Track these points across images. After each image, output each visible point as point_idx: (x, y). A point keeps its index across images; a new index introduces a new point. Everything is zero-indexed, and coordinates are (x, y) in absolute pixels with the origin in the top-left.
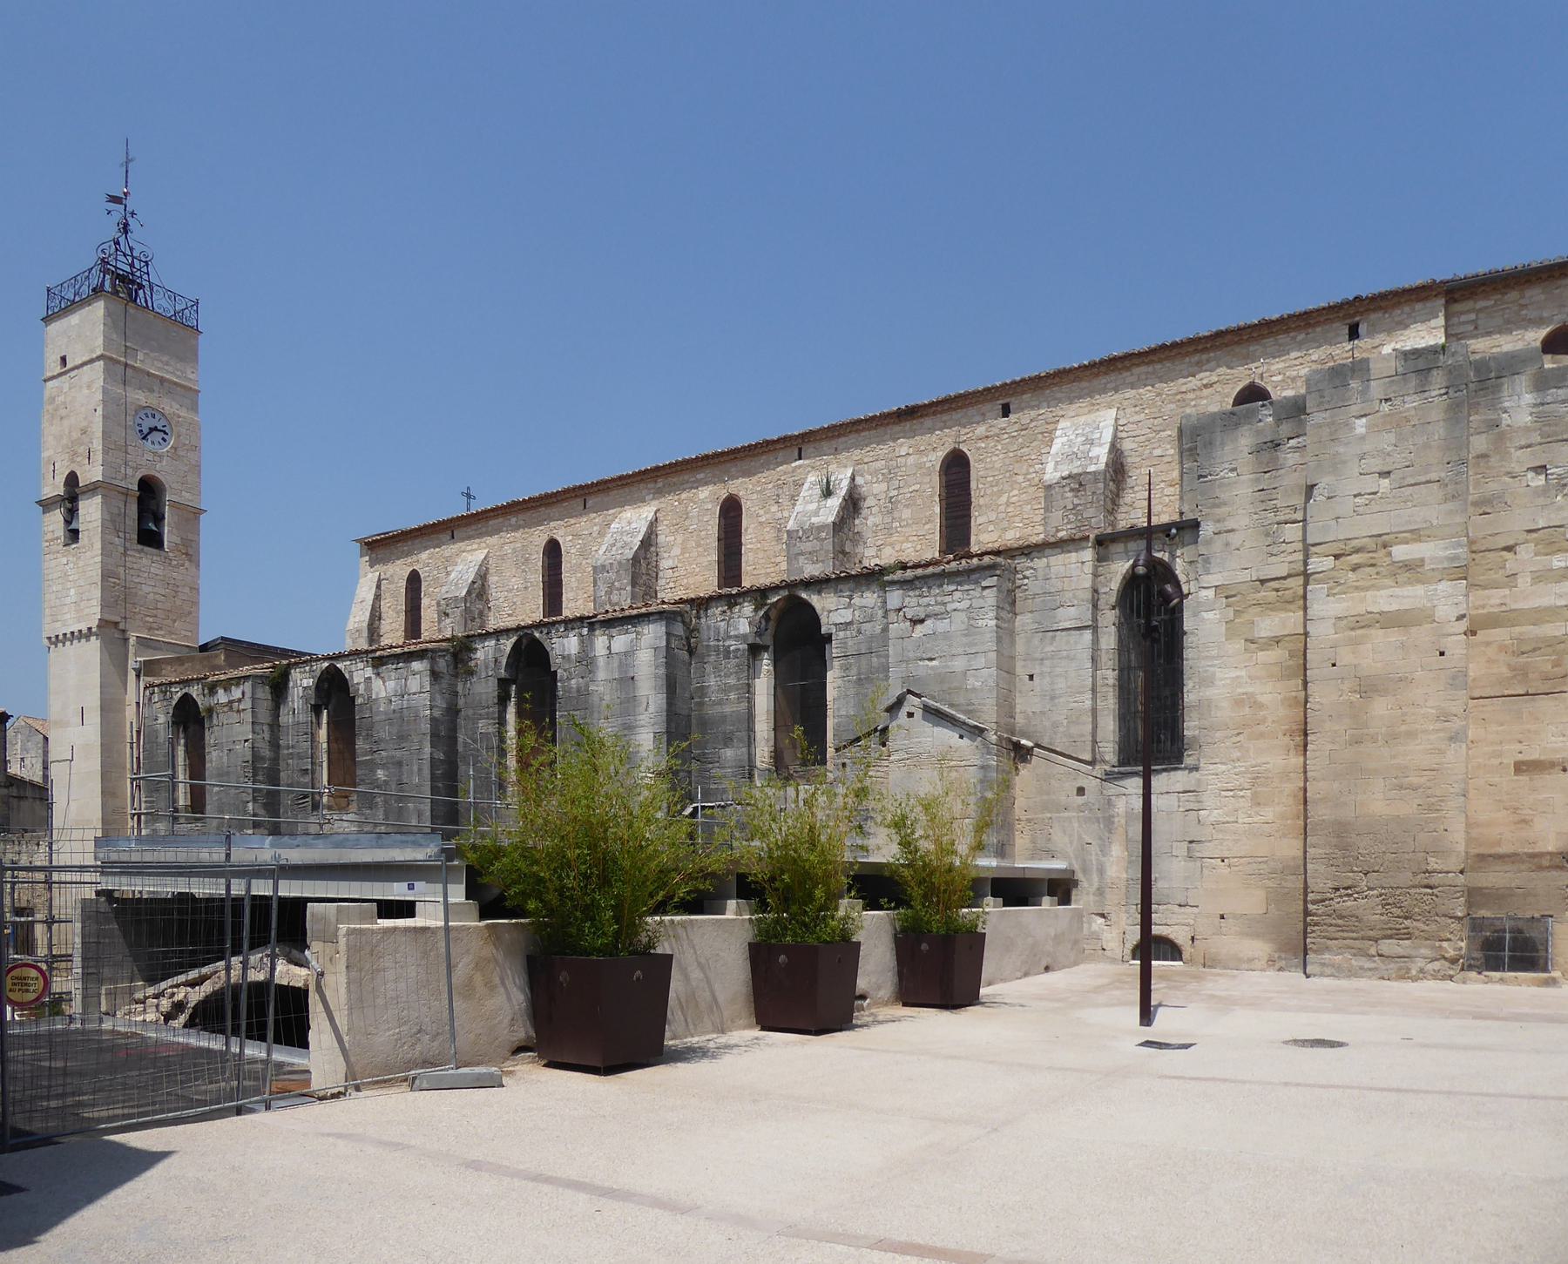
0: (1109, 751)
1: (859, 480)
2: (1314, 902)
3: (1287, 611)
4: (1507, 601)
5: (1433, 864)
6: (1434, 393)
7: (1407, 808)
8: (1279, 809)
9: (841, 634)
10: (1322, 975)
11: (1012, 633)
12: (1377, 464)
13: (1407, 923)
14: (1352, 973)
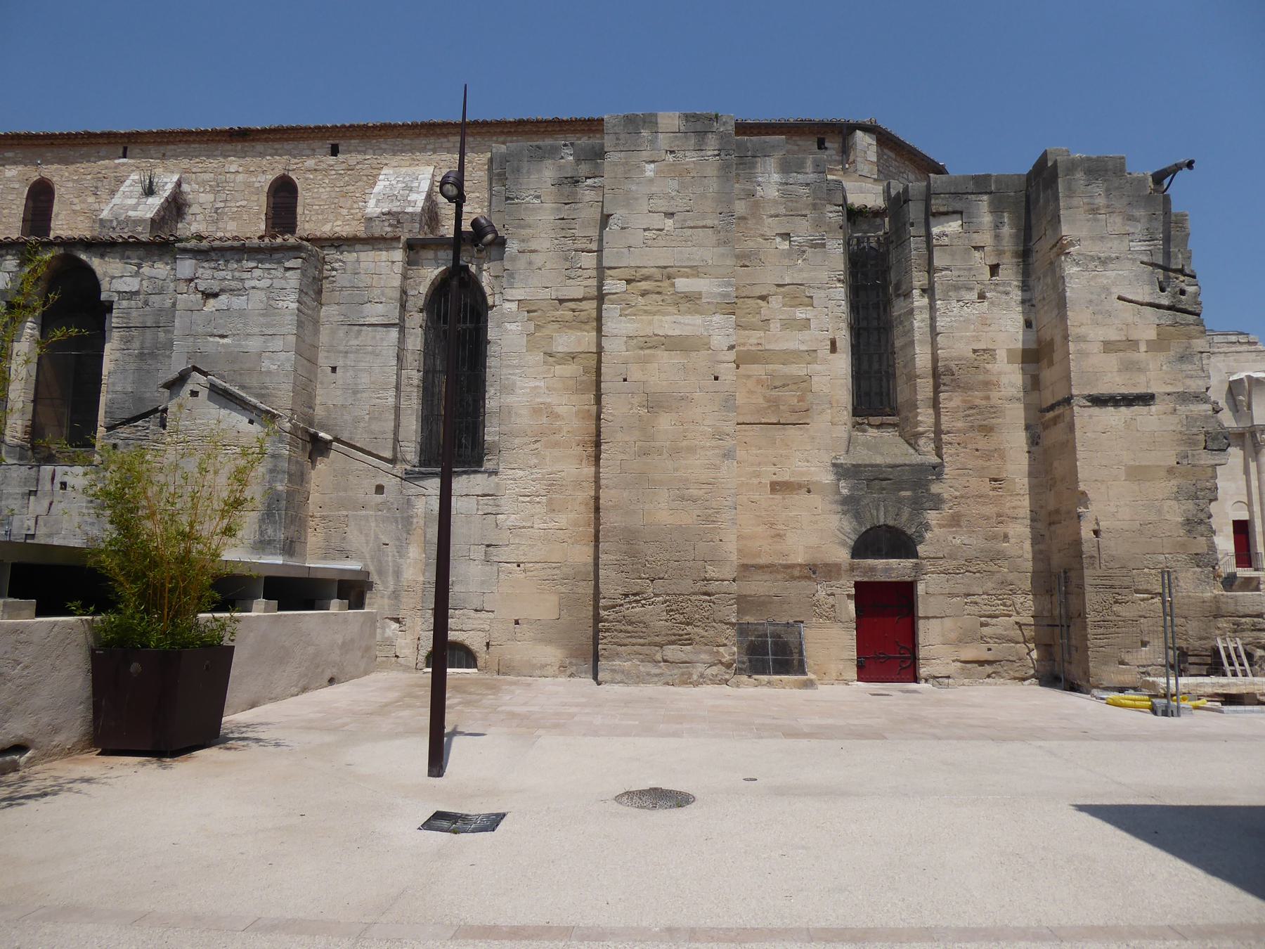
0: (411, 451)
1: (185, 187)
2: (606, 608)
3: (581, 329)
4: (763, 341)
5: (712, 572)
6: (710, 153)
7: (688, 518)
8: (573, 516)
9: (125, 303)
10: (613, 682)
11: (316, 322)
12: (663, 205)
13: (689, 628)
14: (640, 679)
